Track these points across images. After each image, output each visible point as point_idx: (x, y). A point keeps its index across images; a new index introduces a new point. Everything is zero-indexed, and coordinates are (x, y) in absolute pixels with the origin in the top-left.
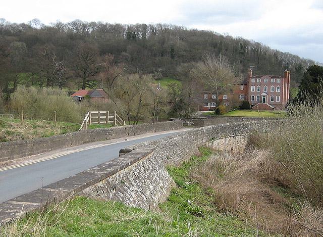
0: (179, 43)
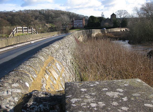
0: (53, 14)
